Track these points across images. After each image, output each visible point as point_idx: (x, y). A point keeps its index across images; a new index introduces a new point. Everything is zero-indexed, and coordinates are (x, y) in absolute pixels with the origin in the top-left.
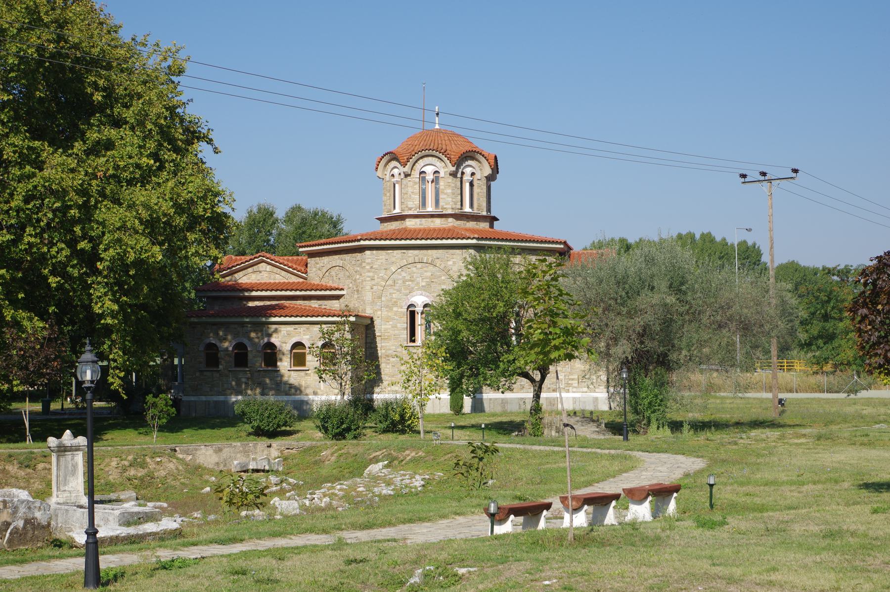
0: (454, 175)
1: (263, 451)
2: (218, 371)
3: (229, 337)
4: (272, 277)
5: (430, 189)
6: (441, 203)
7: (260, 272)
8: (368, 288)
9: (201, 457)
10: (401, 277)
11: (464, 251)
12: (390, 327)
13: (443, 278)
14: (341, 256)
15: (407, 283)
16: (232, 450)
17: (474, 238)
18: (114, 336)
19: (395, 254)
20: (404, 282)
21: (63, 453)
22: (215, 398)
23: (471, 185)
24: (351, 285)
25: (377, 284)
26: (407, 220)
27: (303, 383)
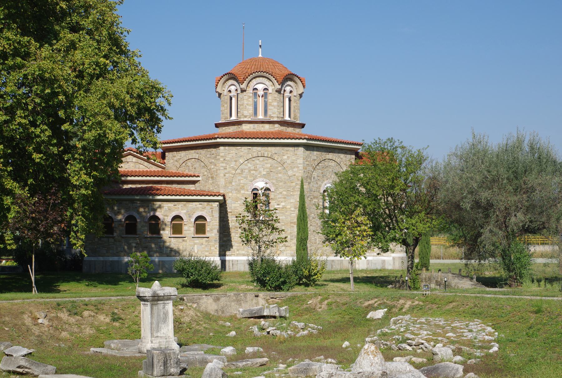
0: (279, 91)
1: (252, 300)
2: (113, 237)
3: (123, 211)
4: (137, 166)
5: (261, 101)
6: (269, 113)
7: (128, 162)
8: (222, 175)
9: (204, 306)
10: (247, 167)
11: (296, 148)
12: (238, 205)
13: (279, 168)
14: (197, 151)
15: (252, 172)
16: (227, 299)
17: (305, 139)
18: (76, 205)
19: (243, 150)
20: (250, 171)
21: (156, 302)
22: (111, 259)
23: (290, 100)
24: (206, 173)
25: (229, 172)
26: (243, 125)
27: (181, 248)
